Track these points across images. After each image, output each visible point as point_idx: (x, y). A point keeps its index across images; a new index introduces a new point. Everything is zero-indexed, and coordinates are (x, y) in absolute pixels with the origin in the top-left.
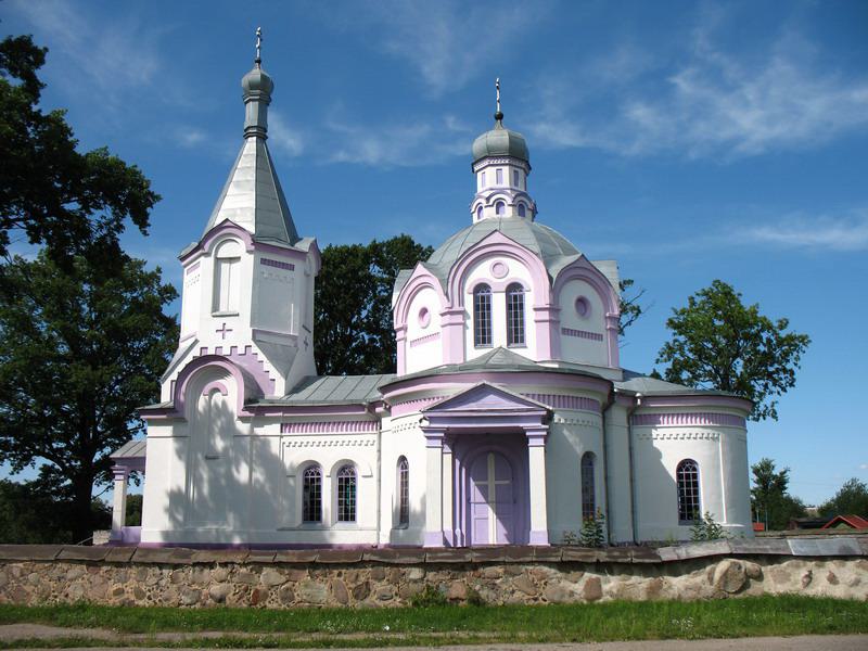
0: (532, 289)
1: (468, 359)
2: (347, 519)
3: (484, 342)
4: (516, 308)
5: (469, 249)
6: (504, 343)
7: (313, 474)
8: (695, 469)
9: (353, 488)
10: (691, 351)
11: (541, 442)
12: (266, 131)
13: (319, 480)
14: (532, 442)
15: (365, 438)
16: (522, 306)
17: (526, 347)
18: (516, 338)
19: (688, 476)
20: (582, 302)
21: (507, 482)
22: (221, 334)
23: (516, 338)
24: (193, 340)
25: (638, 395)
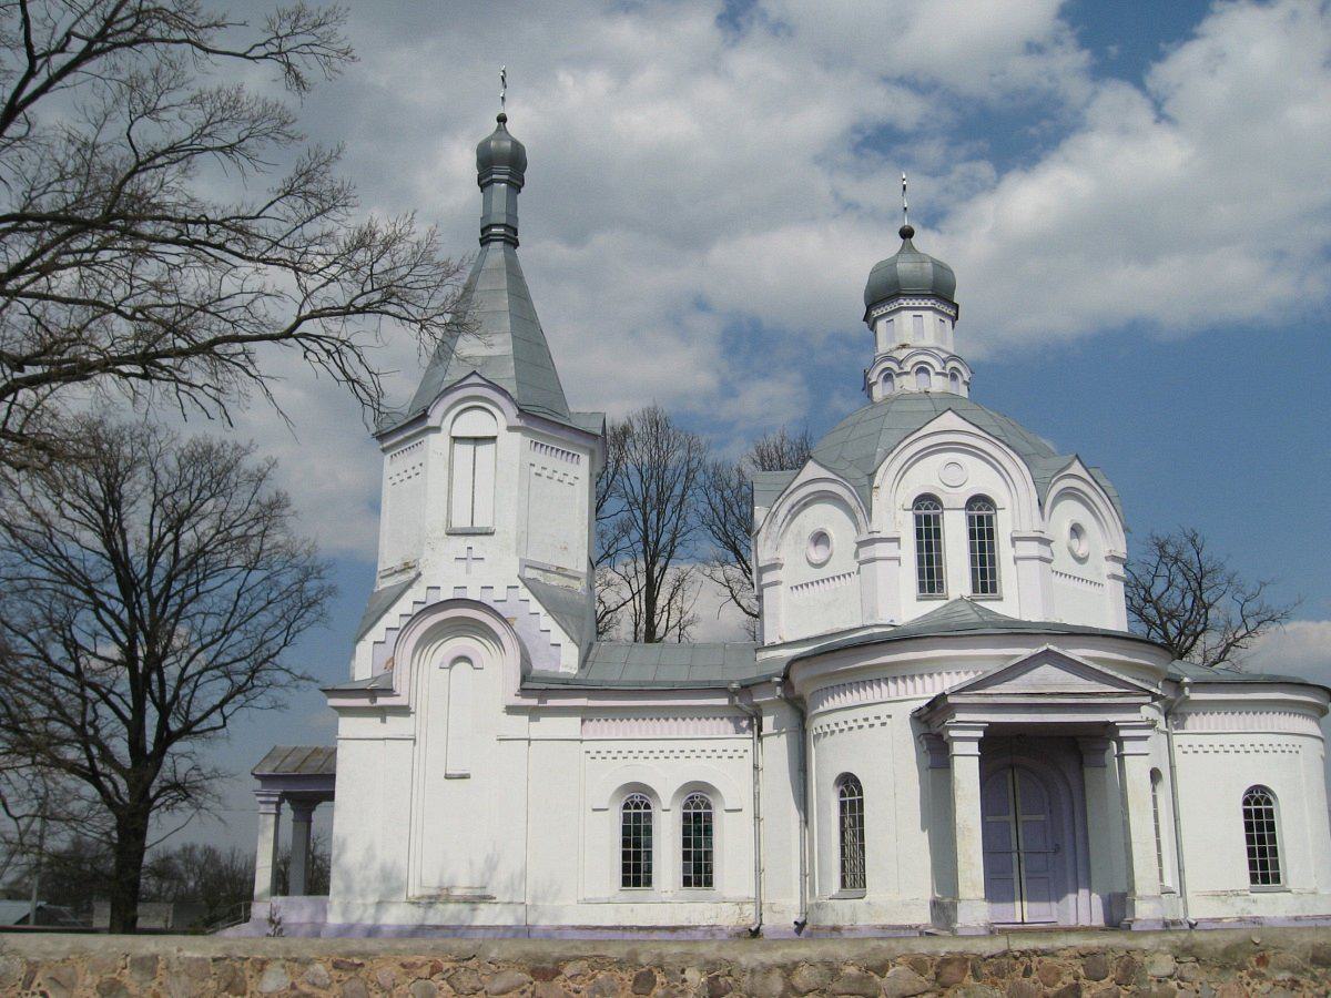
0: (1008, 506)
1: (476, 525)
2: (637, 883)
3: (931, 590)
4: (981, 536)
5: (924, 449)
6: (967, 590)
7: (698, 807)
8: (1268, 802)
9: (708, 830)
10: (152, 182)
11: (974, 748)
12: (516, 233)
13: (649, 816)
14: (957, 747)
15: (730, 745)
16: (991, 533)
17: (1001, 599)
18: (984, 585)
19: (1259, 812)
20: (1076, 531)
21: (1042, 817)
22: (463, 564)
23: (984, 585)
24: (412, 574)
25: (1186, 680)
